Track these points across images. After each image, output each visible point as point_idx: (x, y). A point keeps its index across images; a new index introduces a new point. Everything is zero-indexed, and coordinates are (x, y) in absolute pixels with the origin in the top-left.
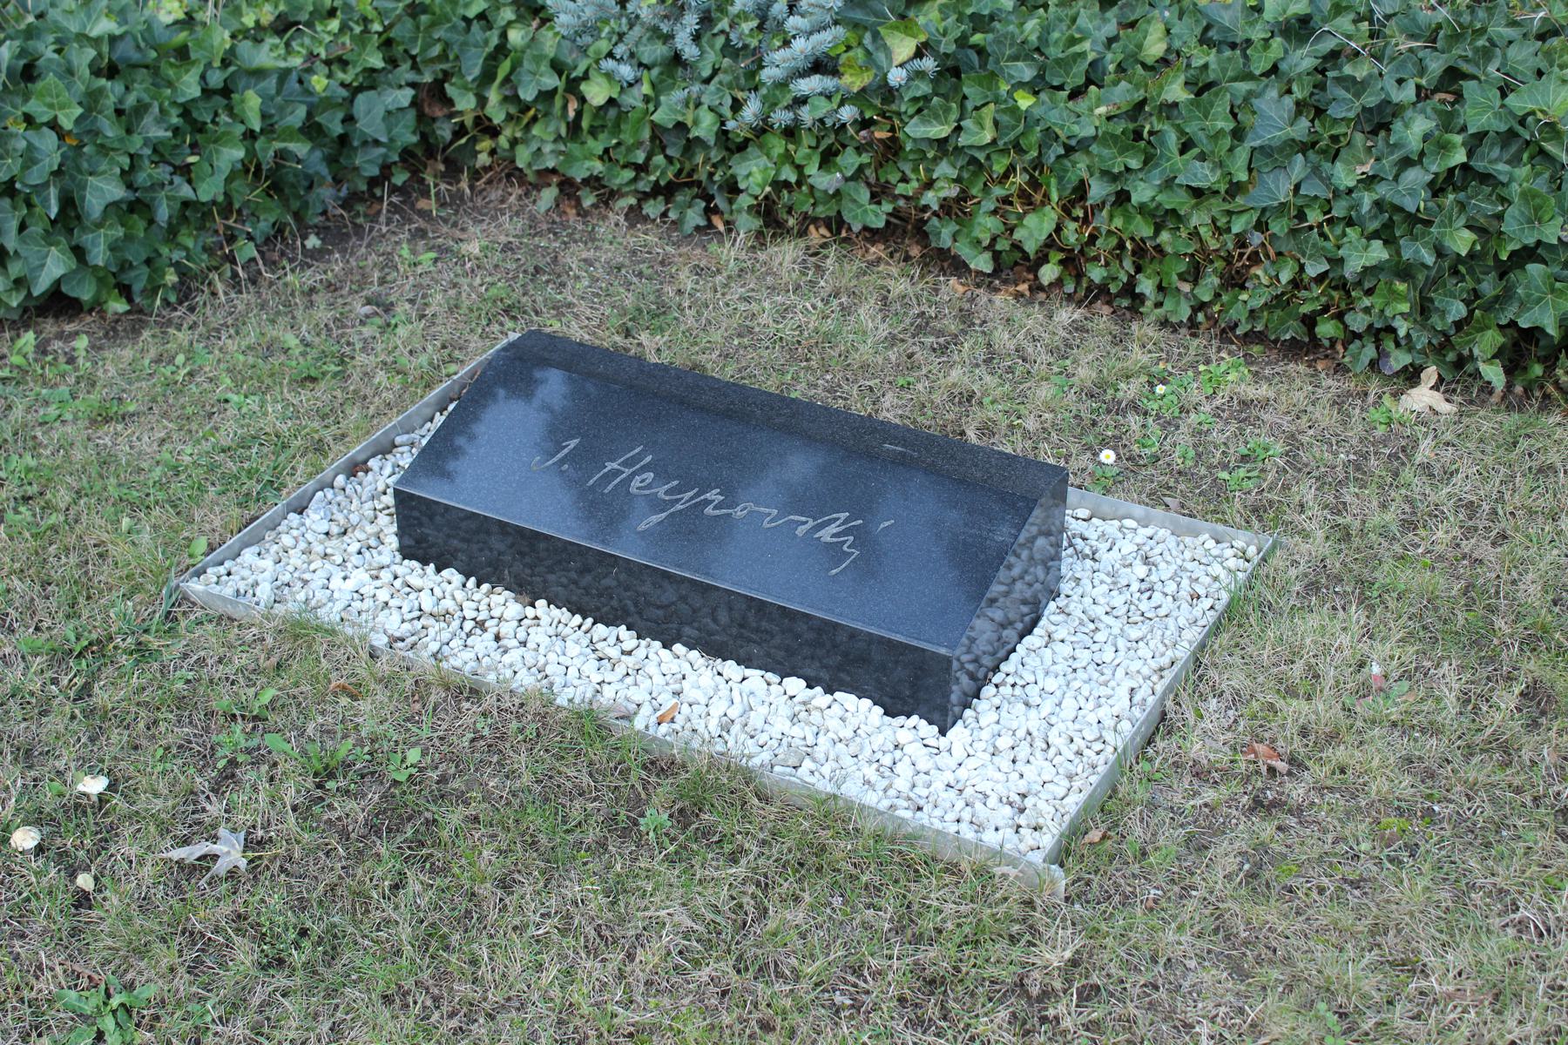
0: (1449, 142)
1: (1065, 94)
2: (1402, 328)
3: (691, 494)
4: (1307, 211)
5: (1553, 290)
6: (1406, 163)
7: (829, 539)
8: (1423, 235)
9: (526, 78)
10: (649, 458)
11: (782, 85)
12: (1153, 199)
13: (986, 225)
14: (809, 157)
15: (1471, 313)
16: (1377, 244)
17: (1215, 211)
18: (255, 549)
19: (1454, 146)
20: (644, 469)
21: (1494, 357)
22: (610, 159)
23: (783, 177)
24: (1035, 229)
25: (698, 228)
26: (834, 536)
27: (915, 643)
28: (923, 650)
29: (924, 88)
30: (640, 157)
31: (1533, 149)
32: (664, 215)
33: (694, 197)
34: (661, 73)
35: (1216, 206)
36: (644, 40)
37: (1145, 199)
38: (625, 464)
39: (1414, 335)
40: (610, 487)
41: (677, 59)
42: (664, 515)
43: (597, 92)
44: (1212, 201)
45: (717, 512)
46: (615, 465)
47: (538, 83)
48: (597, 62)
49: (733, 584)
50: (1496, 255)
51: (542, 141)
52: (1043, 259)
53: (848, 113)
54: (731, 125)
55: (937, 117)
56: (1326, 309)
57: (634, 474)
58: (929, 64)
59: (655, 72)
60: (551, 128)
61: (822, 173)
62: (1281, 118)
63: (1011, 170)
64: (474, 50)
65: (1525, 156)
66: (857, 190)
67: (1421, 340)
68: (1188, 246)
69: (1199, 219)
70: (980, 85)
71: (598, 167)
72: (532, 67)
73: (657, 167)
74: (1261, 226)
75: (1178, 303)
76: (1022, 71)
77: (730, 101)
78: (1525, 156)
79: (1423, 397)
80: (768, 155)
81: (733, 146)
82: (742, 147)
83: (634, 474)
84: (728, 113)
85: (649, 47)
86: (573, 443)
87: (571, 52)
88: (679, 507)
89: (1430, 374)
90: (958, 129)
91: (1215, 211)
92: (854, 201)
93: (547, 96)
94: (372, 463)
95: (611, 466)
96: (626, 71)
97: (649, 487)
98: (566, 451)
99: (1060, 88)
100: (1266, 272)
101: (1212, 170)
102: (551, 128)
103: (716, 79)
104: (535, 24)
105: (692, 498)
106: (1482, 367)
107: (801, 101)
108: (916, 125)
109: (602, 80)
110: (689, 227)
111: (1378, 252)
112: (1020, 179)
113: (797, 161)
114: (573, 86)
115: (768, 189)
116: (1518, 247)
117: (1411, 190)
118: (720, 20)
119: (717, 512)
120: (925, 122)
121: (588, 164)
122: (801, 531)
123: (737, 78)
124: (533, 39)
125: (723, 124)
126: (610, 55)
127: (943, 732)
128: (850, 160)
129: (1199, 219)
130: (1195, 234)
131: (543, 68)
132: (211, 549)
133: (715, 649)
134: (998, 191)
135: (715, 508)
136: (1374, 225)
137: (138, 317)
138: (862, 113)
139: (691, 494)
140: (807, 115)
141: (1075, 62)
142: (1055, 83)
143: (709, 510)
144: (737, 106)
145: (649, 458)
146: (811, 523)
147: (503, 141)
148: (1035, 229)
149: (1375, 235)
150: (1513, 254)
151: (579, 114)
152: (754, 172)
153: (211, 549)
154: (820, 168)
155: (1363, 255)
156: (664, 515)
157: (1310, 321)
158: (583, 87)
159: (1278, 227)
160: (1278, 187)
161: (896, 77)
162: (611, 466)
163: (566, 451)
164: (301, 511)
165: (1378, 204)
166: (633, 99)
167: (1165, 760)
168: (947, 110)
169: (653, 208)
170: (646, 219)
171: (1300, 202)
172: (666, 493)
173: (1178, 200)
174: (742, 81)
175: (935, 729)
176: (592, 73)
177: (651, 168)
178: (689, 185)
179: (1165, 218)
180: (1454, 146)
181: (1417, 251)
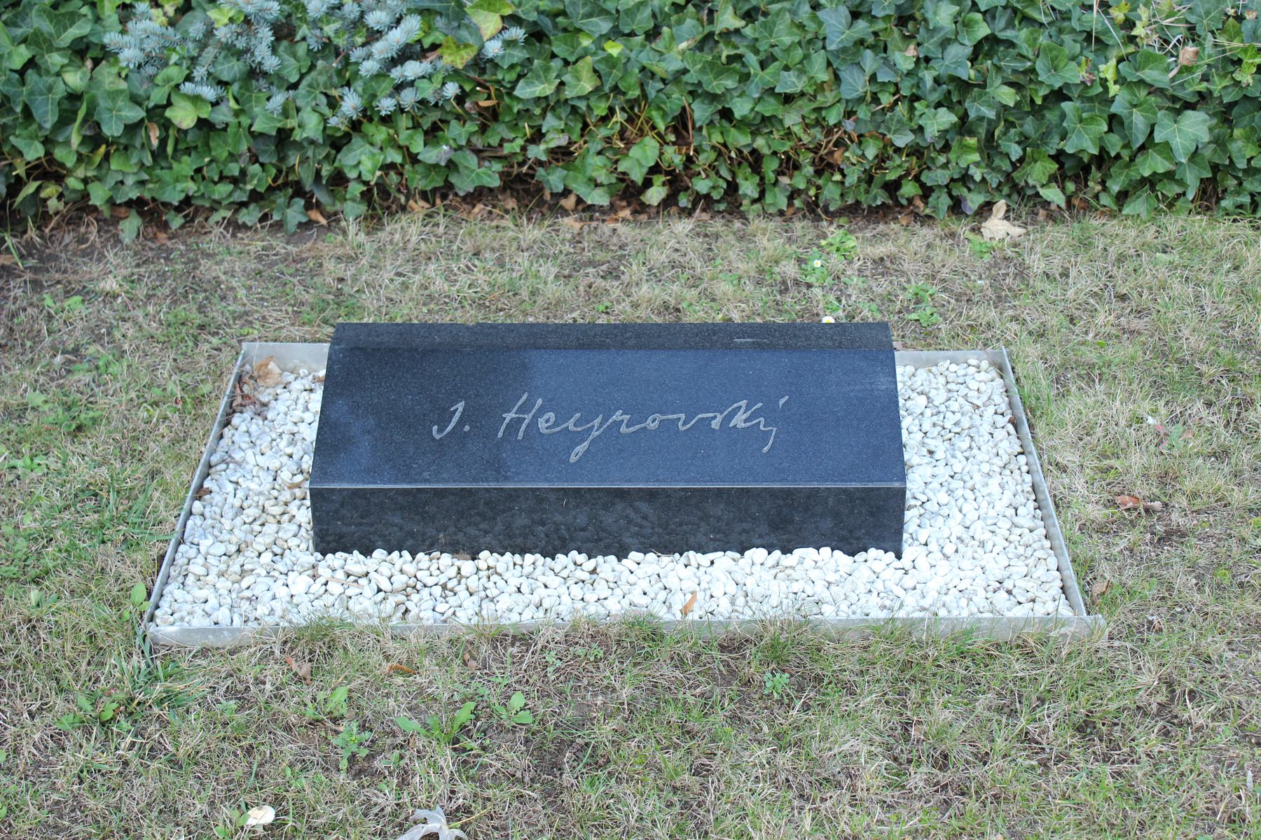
0: (971, 20)
2: (977, 174)
4: (880, 95)
5: (1081, 121)
6: (945, 43)
7: (744, 425)
8: (980, 96)
9: (106, 116)
10: (540, 401)
11: (381, 75)
12: (753, 109)
13: (597, 166)
14: (411, 137)
15: (1024, 150)
16: (943, 111)
17: (806, 111)
19: (976, 22)
20: (542, 411)
21: (1050, 181)
22: (204, 178)
23: (389, 160)
24: (644, 154)
25: (300, 225)
26: (745, 421)
27: (870, 485)
28: (879, 489)
29: (518, 55)
30: (234, 169)
31: (1019, 16)
32: (264, 218)
33: (292, 197)
34: (241, 88)
35: (805, 107)
36: (221, 58)
39: (988, 177)
40: (521, 435)
41: (254, 73)
42: (586, 444)
43: (184, 117)
44: (800, 103)
45: (632, 429)
47: (119, 118)
48: (177, 86)
49: (688, 481)
50: (1032, 101)
51: (124, 173)
52: (648, 183)
53: (452, 89)
54: (333, 121)
55: (538, 77)
56: (908, 173)
57: (535, 418)
58: (518, 33)
59: (235, 88)
60: (134, 160)
61: (428, 148)
62: (840, 23)
63: (611, 111)
64: (40, 98)
65: (1016, 22)
66: (465, 158)
67: (994, 180)
68: (783, 145)
69: (792, 119)
71: (191, 187)
72: (110, 104)
73: (253, 176)
74: (849, 114)
75: (775, 196)
76: (597, 25)
77: (324, 100)
78: (1016, 22)
79: (998, 227)
80: (372, 144)
81: (337, 143)
82: (347, 137)
83: (535, 418)
84: (327, 111)
85: (226, 66)
86: (460, 406)
87: (142, 84)
88: (595, 434)
89: (1001, 206)
91: (806, 111)
92: (467, 168)
93: (132, 129)
94: (207, 484)
95: (509, 416)
96: (209, 93)
97: (556, 424)
98: (458, 415)
99: (632, 34)
100: (854, 153)
101: (798, 77)
102: (134, 160)
103: (304, 83)
104: (89, 63)
105: (601, 424)
106: (1042, 192)
107: (399, 88)
108: (522, 88)
109: (188, 105)
111: (946, 118)
112: (619, 117)
113: (402, 143)
114: (157, 114)
115: (378, 173)
116: (1047, 92)
117: (956, 61)
118: (300, 27)
119: (632, 429)
120: (529, 84)
121: (180, 186)
122: (715, 424)
123: (330, 78)
124: (91, 78)
125: (325, 120)
126: (189, 78)
127: (899, 557)
128: (457, 132)
129: (792, 119)
130: (789, 134)
131: (120, 104)
133: (669, 545)
134: (603, 132)
135: (628, 426)
136: (935, 97)
138: (461, 87)
140: (408, 98)
141: (638, 9)
142: (627, 31)
144: (333, 103)
145: (540, 401)
146: (720, 418)
147: (73, 183)
148: (644, 154)
149: (939, 105)
150: (1045, 98)
151: (163, 142)
154: (425, 144)
155: (940, 121)
156: (586, 444)
157: (892, 188)
158: (168, 113)
159: (863, 112)
160: (855, 84)
161: (493, 48)
162: (509, 416)
163: (458, 415)
165: (937, 81)
166: (222, 116)
168: (547, 70)
169: (249, 216)
170: (245, 227)
171: (875, 89)
173: (770, 107)
174: (335, 80)
175: (891, 555)
176: (174, 99)
178: (286, 184)
179: (760, 125)
180: (976, 22)
181: (978, 110)
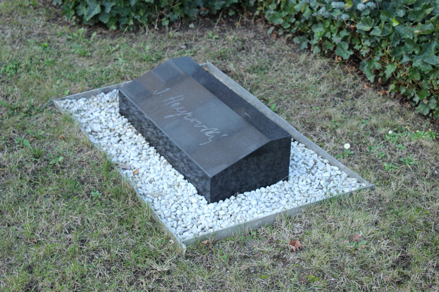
1: (412, 24)
3: (184, 112)
18: (85, 99)
37: (417, 66)
38: (176, 99)
42: (173, 116)
46: (173, 98)
70: (387, 15)
81: (315, 21)
88: (179, 115)
90: (372, 29)
108: (361, 25)
110: (302, 48)
132: (69, 94)
135: (187, 118)
137: (118, 33)
139: (184, 112)
141: (420, 13)
143: (185, 118)
145: (182, 99)
152: (318, 31)
153: (69, 94)
164: (106, 93)
167: (264, 234)
168: (371, 22)
172: (179, 110)
175: (207, 202)
177: (295, 25)
